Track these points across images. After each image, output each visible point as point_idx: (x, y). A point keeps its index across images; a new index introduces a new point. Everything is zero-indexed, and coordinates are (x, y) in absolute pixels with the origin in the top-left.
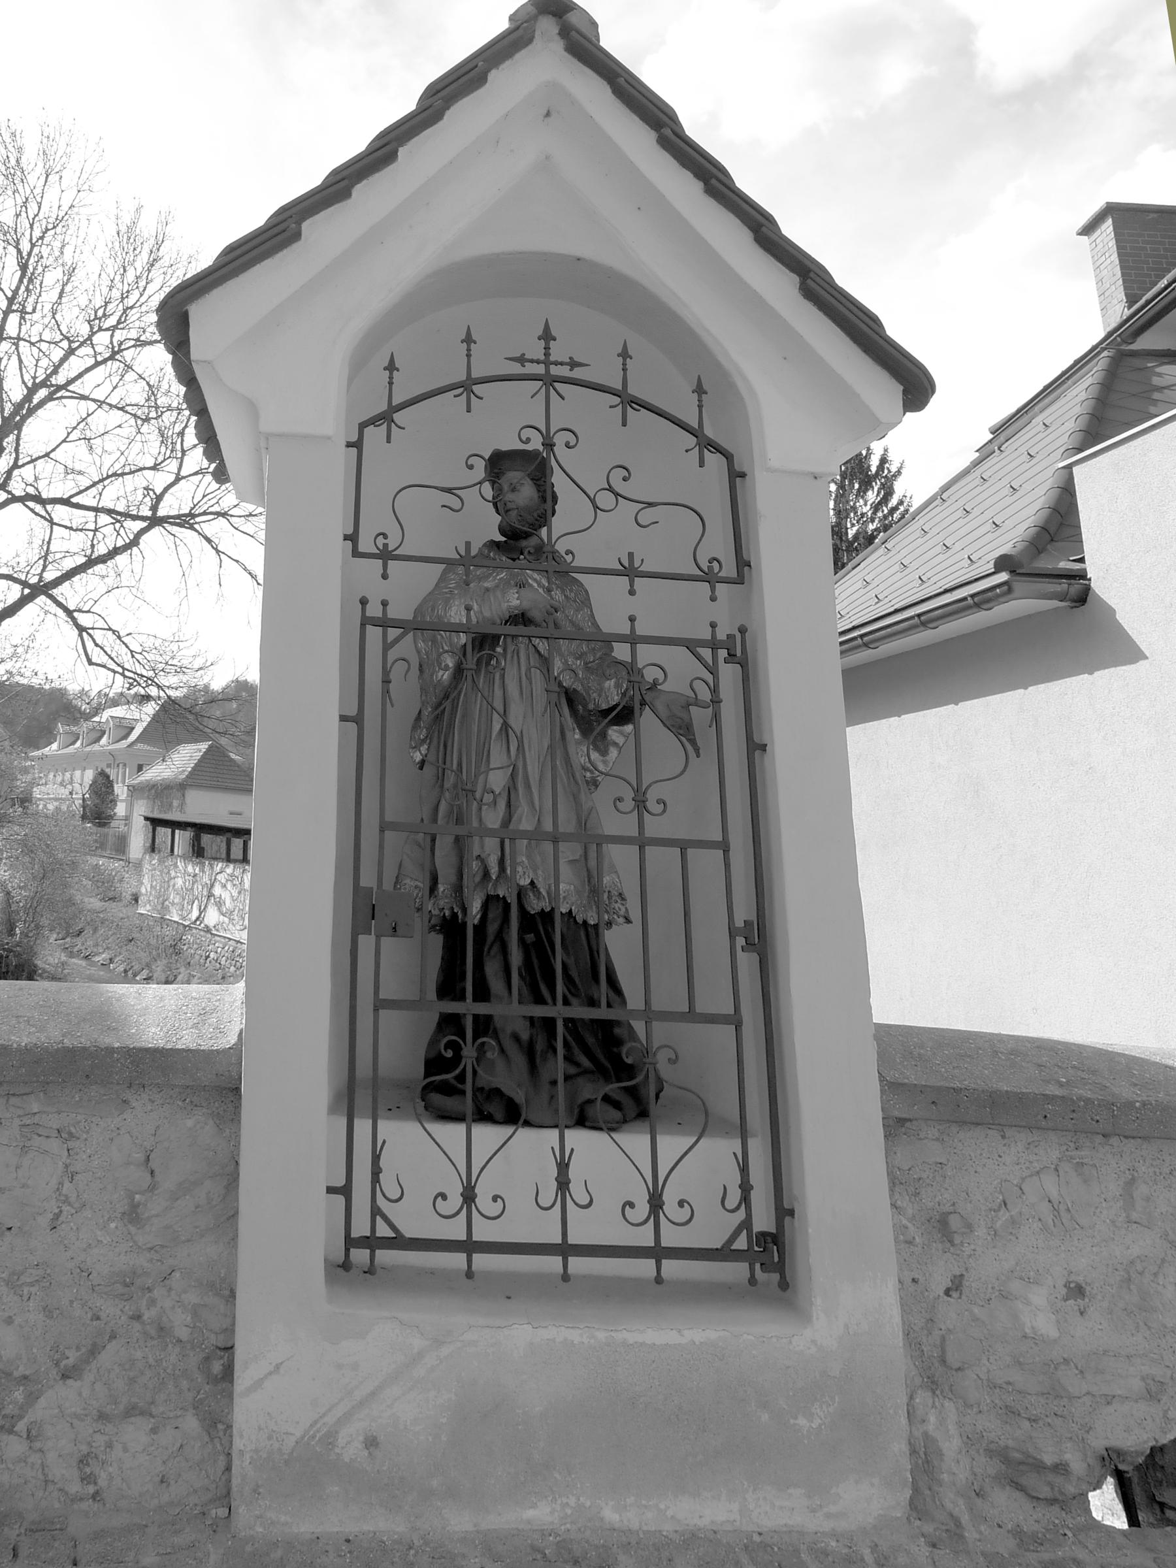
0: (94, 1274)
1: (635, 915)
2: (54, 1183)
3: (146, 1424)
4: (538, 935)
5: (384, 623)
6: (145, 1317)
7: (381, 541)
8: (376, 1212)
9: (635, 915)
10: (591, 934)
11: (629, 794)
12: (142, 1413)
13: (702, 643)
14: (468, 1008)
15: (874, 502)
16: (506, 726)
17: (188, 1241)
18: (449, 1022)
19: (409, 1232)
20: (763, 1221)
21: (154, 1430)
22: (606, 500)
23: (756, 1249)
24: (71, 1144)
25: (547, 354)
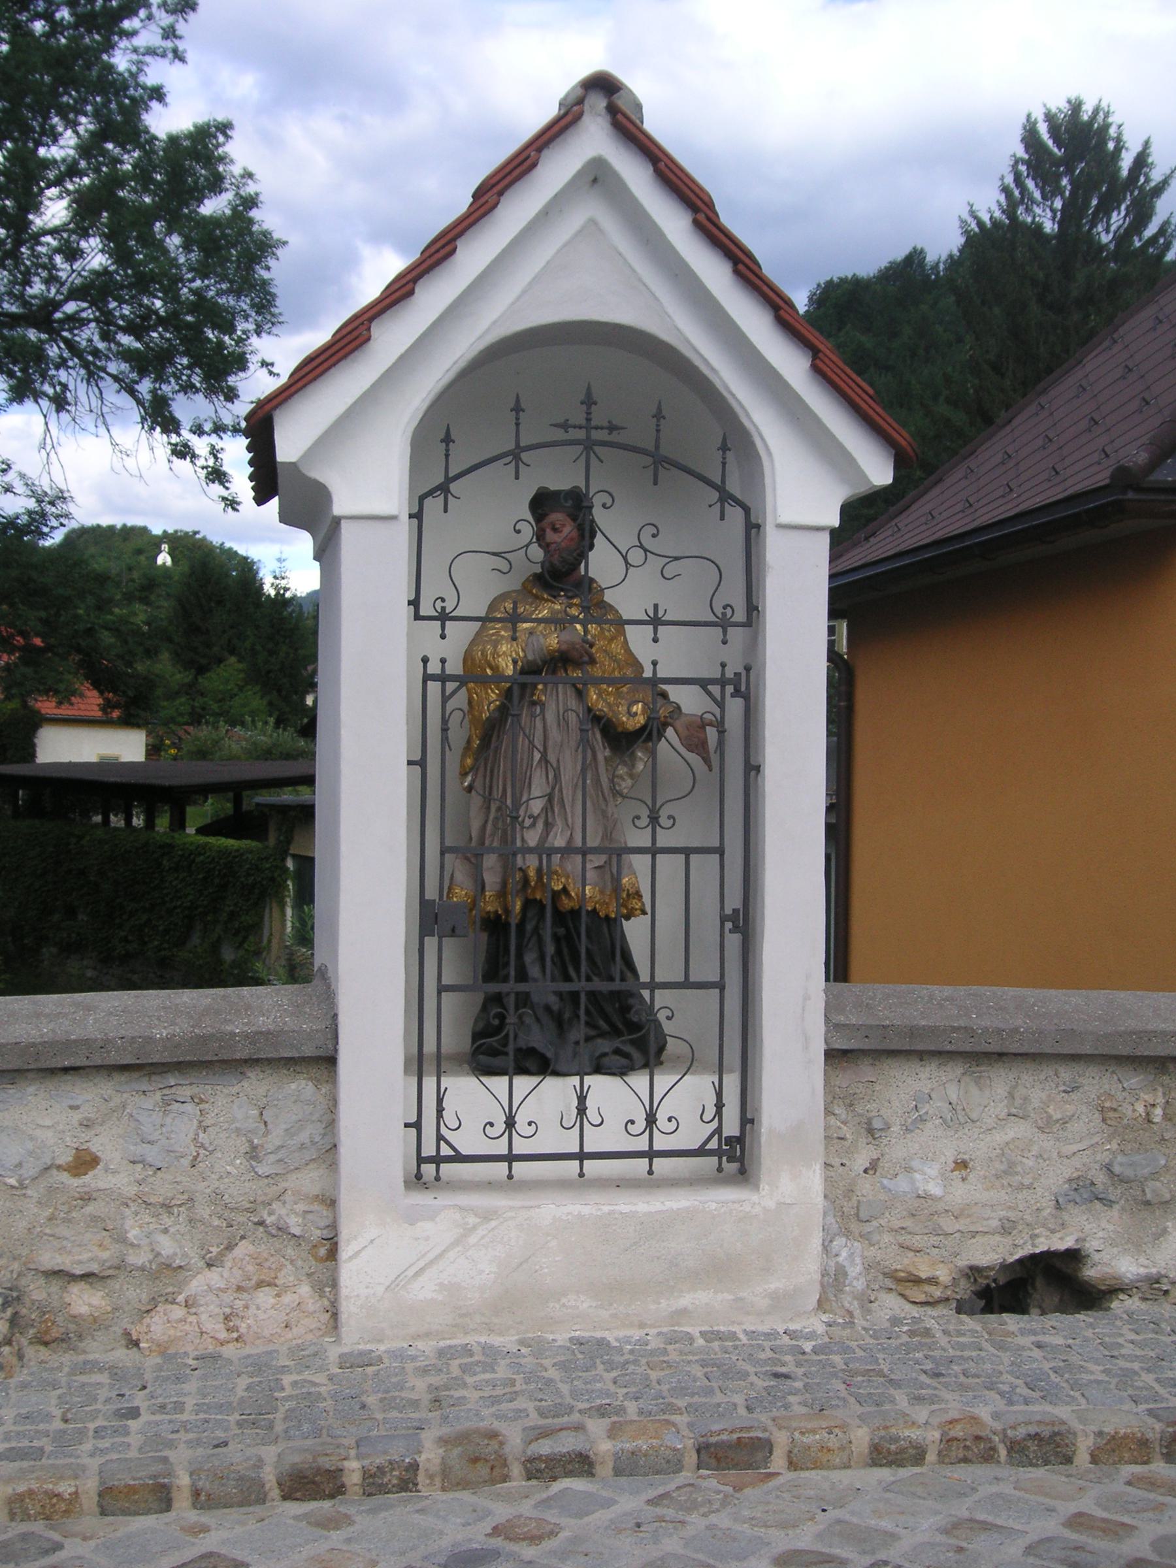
0: (226, 1196)
1: (648, 909)
2: (191, 1136)
3: (274, 1291)
4: (568, 929)
5: (443, 678)
6: (267, 1222)
7: (439, 604)
8: (440, 1138)
9: (648, 909)
10: (612, 924)
11: (645, 813)
12: (269, 1285)
13: (712, 681)
14: (510, 987)
15: (1120, 226)
16: (544, 755)
17: (297, 1169)
18: (496, 999)
19: (464, 1151)
20: (731, 1128)
21: (278, 1295)
22: (636, 556)
23: (724, 1147)
24: (202, 1106)
25: (588, 420)
